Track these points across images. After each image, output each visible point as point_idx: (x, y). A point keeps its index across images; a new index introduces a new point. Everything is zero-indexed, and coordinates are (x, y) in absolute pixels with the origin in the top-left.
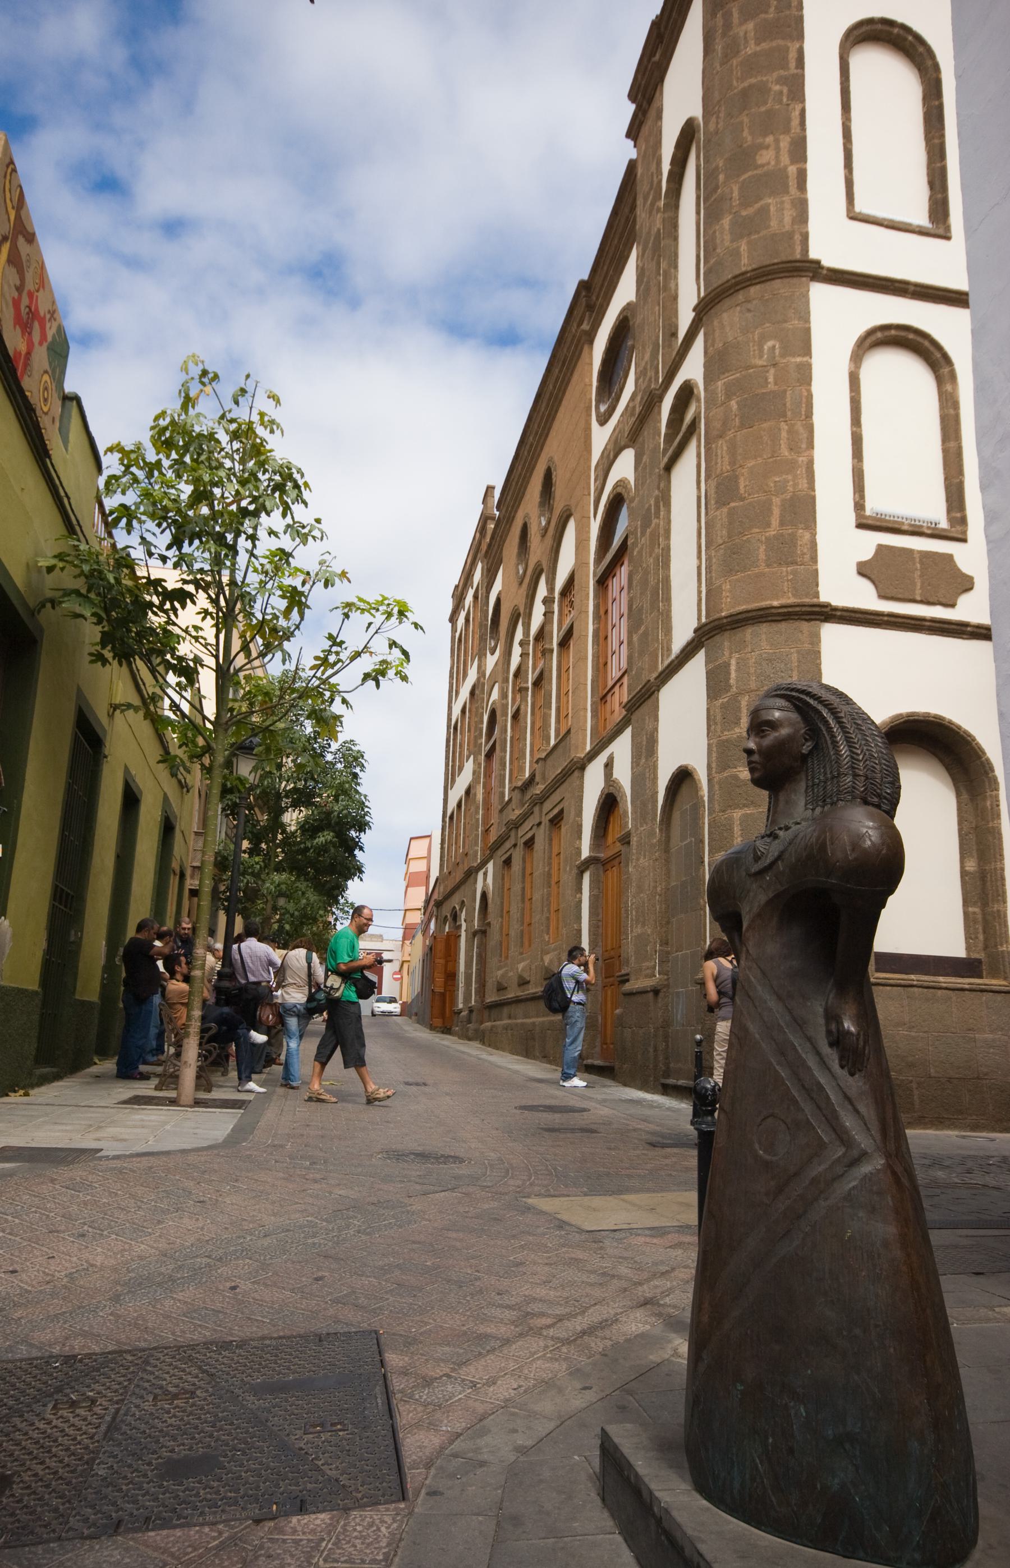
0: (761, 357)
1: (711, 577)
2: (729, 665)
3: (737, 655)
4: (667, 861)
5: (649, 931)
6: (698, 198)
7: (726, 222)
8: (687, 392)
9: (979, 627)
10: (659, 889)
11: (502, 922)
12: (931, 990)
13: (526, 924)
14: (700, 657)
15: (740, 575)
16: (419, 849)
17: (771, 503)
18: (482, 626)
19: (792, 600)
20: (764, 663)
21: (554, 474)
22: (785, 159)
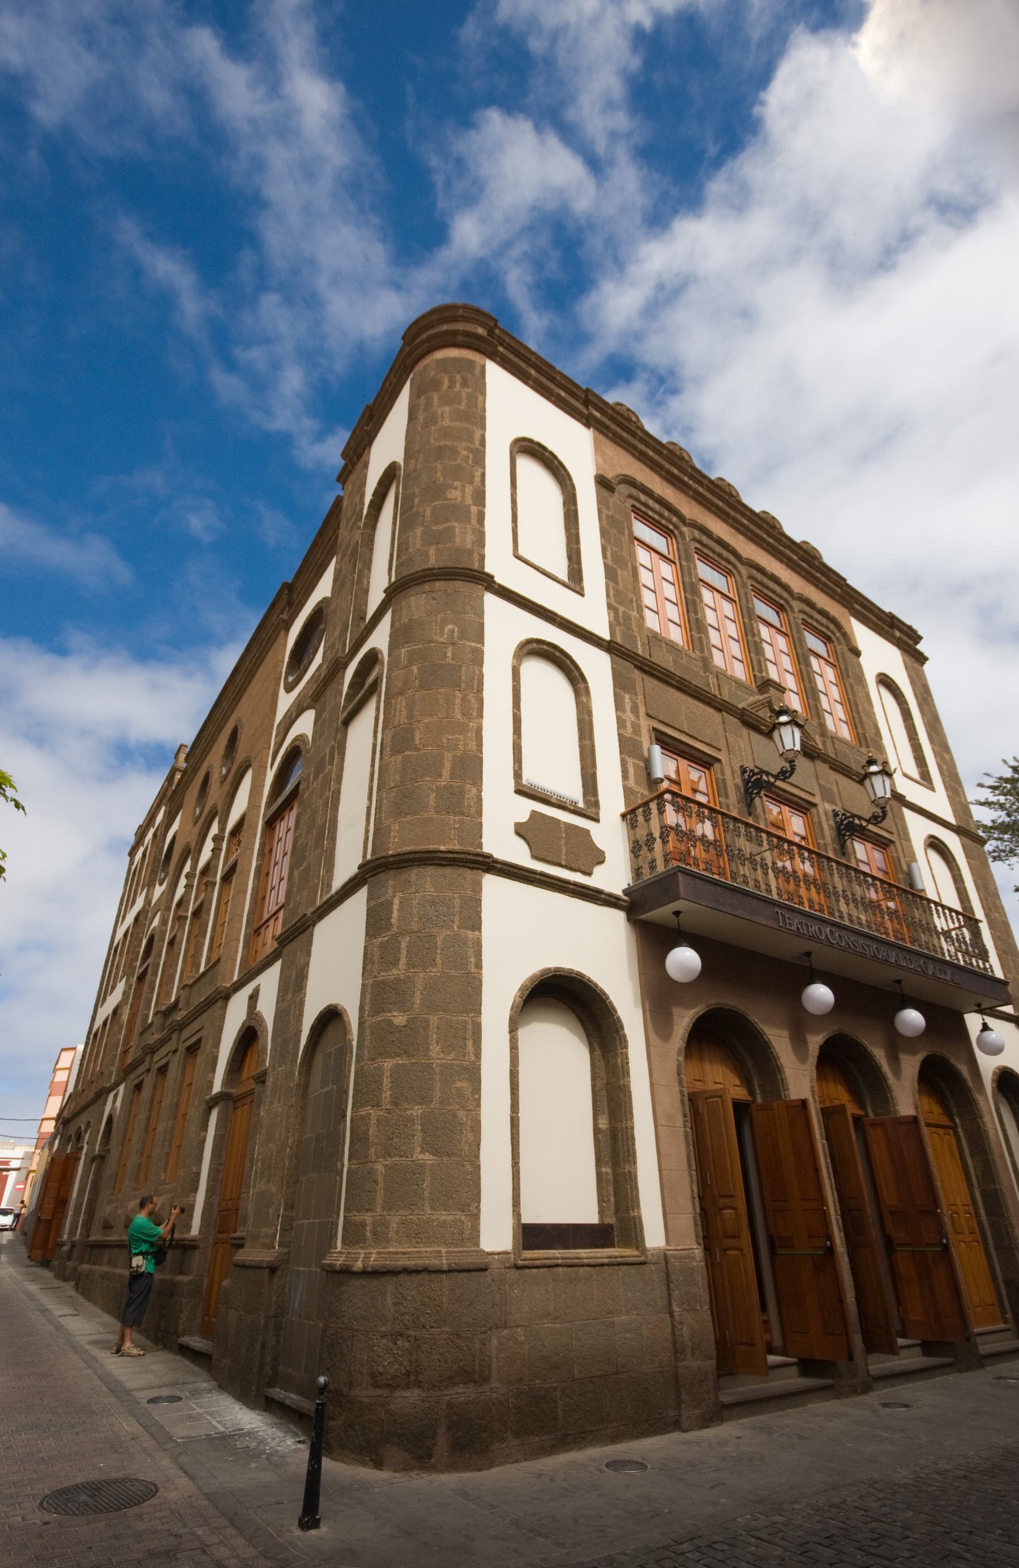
0: (442, 636)
1: (381, 817)
2: (392, 904)
3: (401, 895)
4: (304, 1108)
5: (274, 1190)
6: (395, 514)
7: (419, 531)
9: (610, 895)
10: (290, 1141)
11: (122, 1151)
12: (575, 1269)
14: (362, 894)
15: (409, 818)
18: (156, 860)
19: (457, 847)
21: (240, 731)
22: (469, 500)
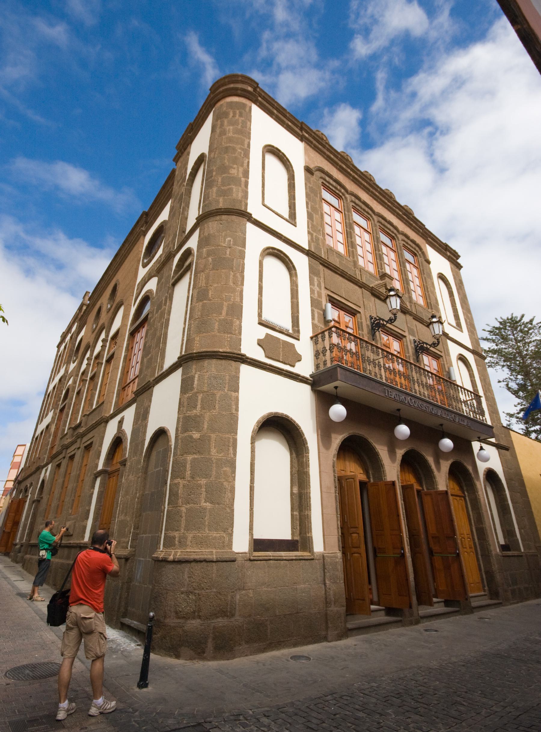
0: (224, 243)
1: (190, 333)
3: (199, 373)
4: (145, 479)
7: (215, 189)
8: (189, 252)
9: (303, 377)
11: (49, 498)
12: (279, 561)
13: (61, 501)
14: (179, 372)
15: (205, 334)
16: (20, 451)
17: (223, 304)
18: (71, 350)
19: (228, 350)
20: (212, 379)
21: (118, 286)
22: (241, 175)
